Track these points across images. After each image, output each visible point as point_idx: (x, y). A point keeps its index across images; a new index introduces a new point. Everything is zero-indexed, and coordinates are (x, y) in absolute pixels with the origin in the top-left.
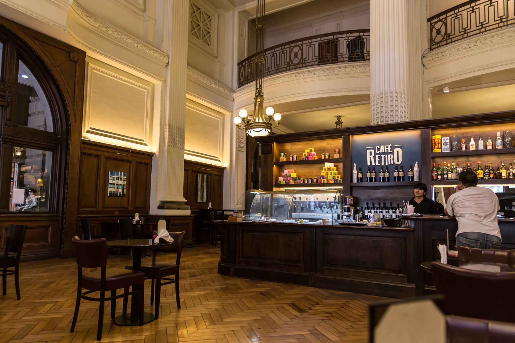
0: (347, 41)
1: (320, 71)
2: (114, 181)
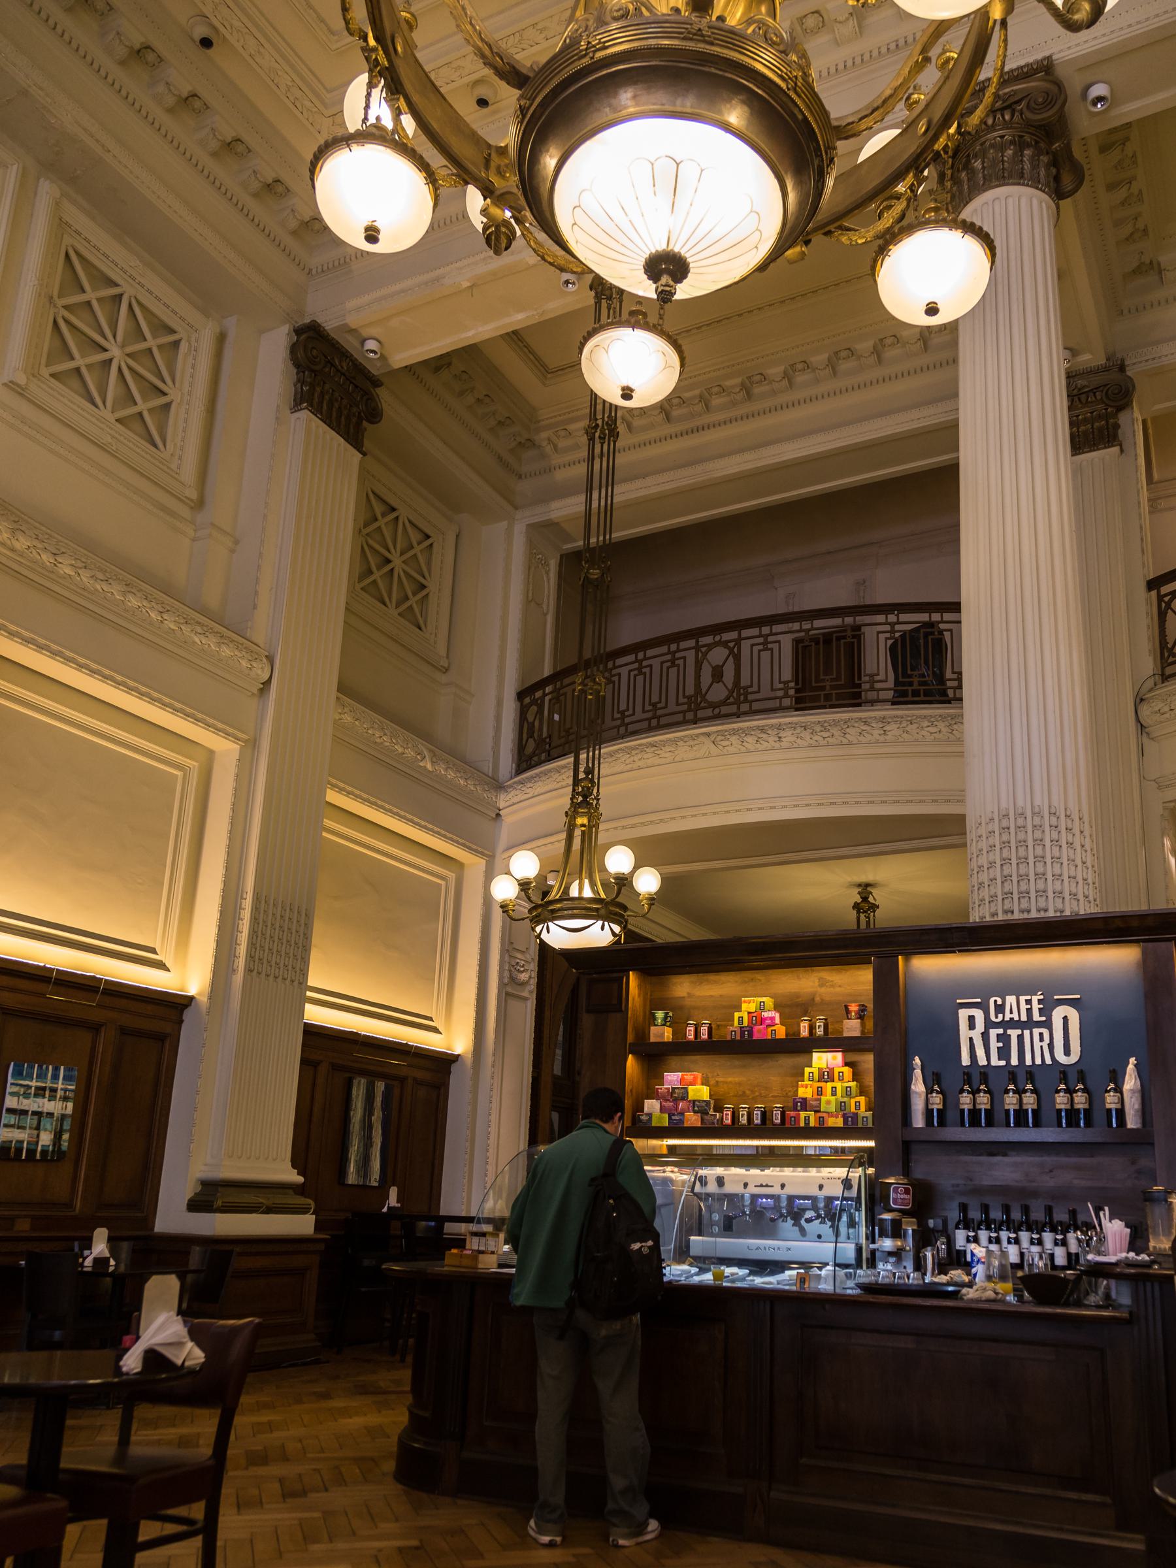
0: (888, 635)
1: (798, 730)
2: (25, 1101)
